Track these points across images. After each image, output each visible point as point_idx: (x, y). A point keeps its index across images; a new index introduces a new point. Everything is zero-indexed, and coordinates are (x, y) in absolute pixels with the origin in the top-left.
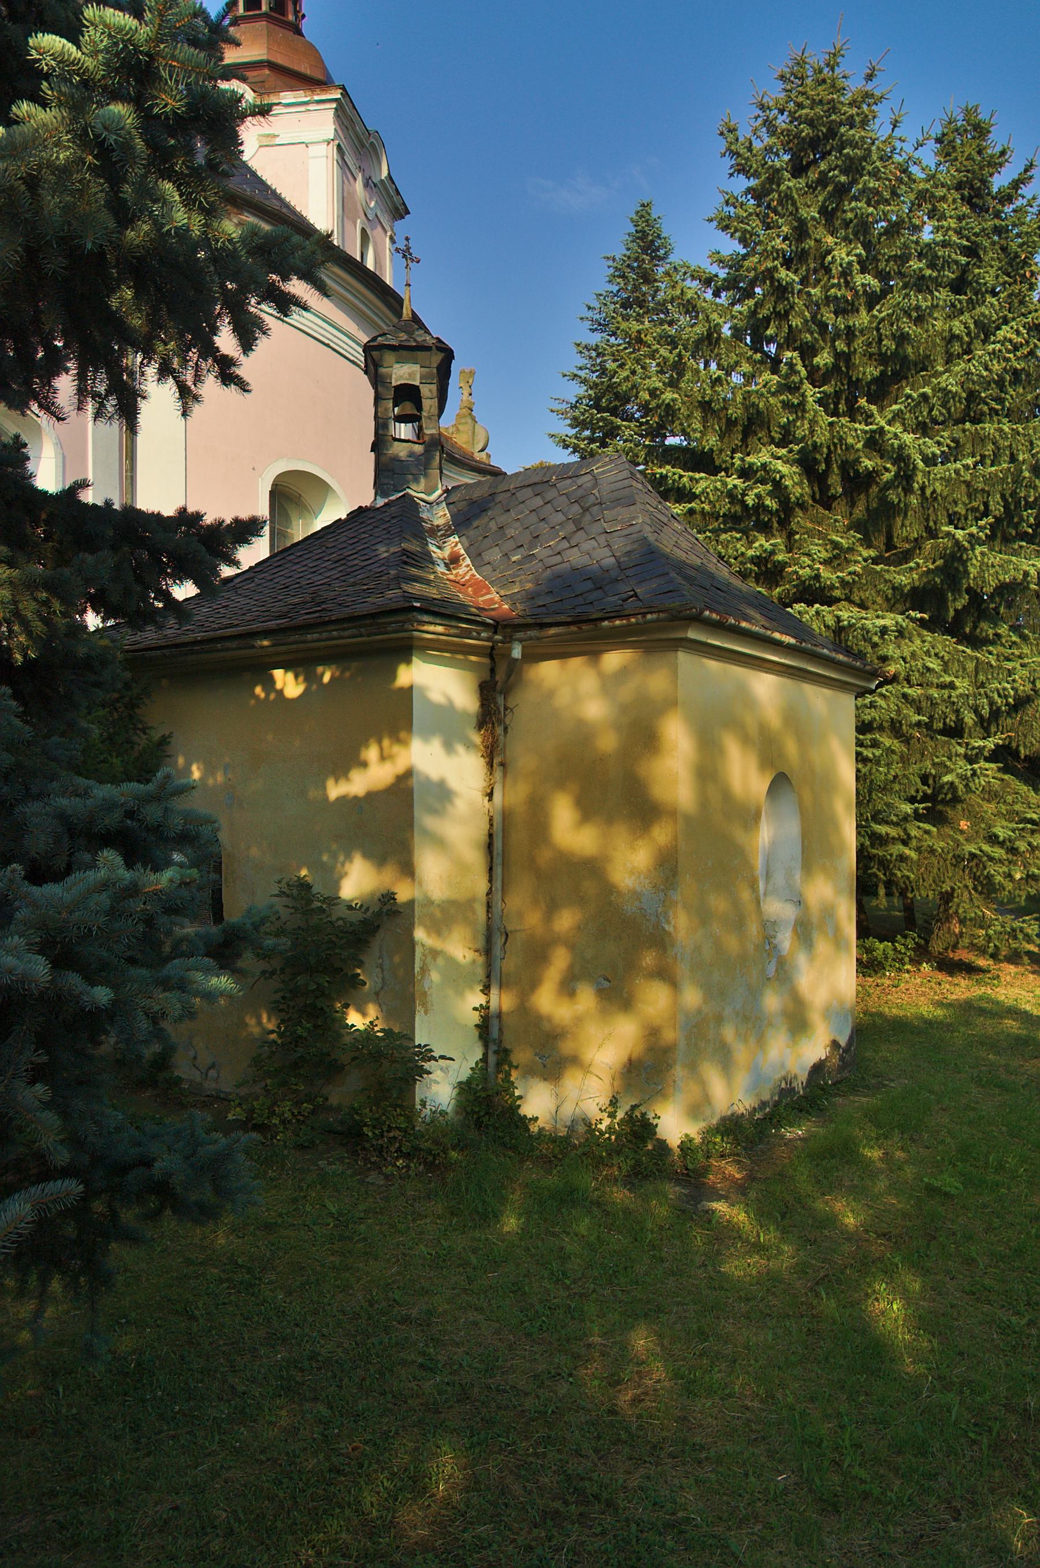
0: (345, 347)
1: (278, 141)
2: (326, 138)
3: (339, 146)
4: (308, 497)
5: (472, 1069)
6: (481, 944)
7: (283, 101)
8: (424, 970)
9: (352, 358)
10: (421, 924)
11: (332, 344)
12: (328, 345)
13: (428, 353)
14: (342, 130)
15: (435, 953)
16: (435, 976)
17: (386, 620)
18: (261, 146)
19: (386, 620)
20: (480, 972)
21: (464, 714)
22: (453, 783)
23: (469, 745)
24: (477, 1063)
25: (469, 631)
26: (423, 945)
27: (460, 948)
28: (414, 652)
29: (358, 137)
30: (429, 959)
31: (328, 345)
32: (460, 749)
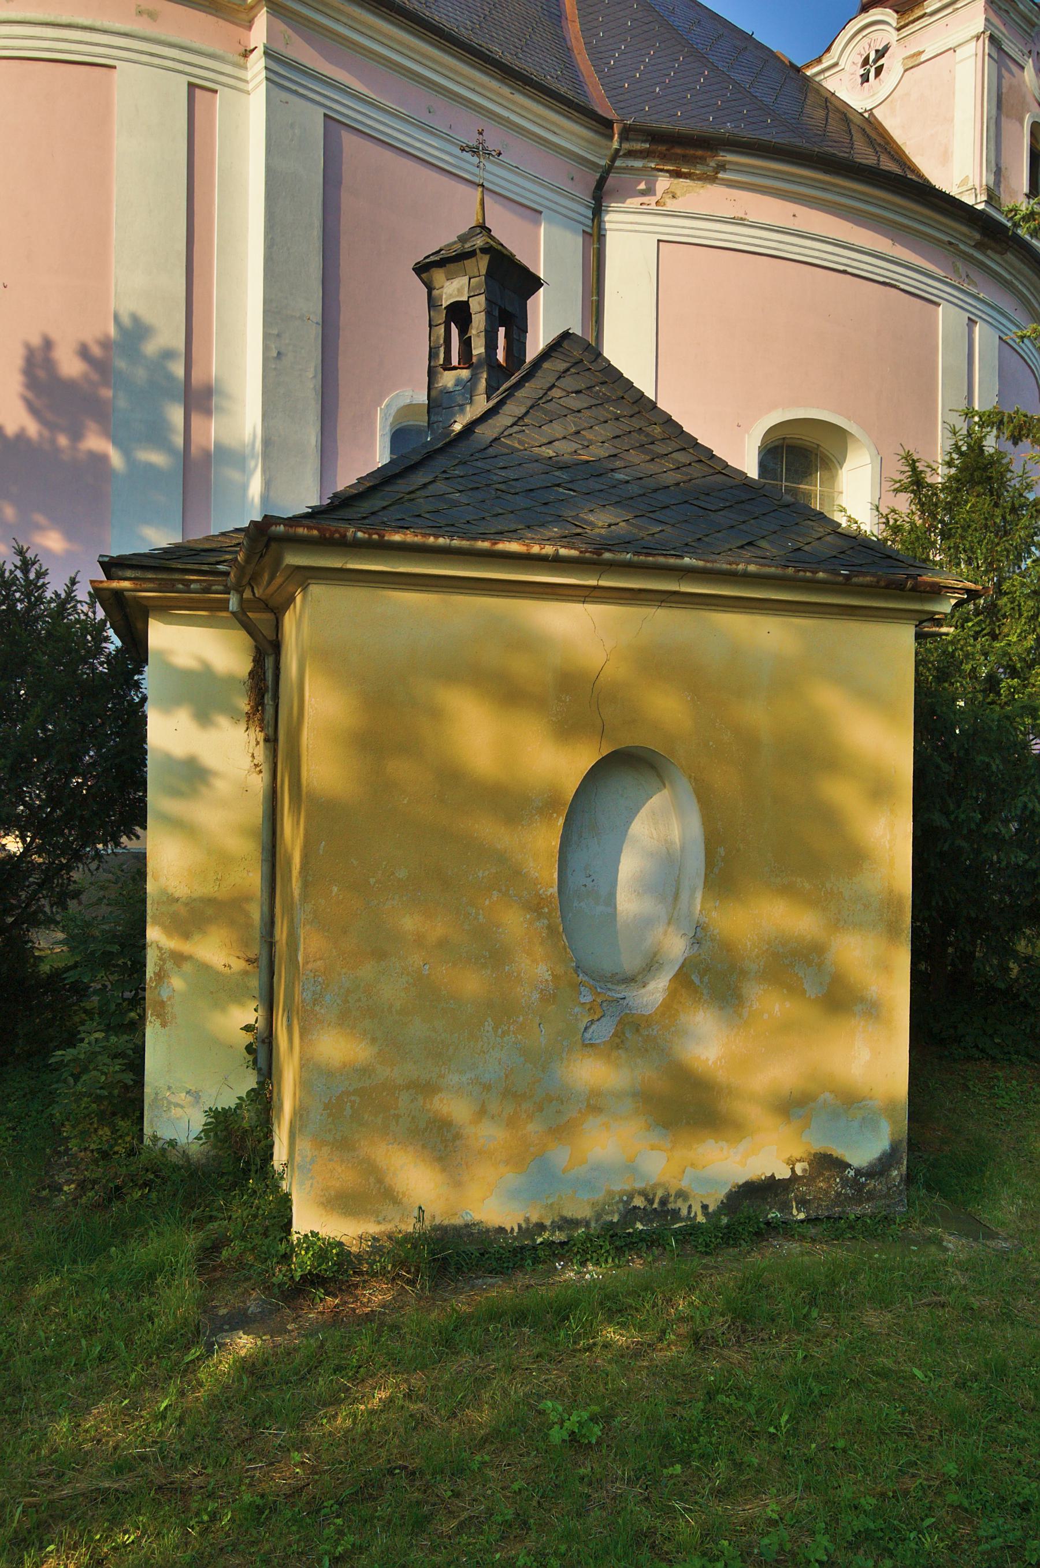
0: (870, 268)
1: (923, 58)
2: (974, 33)
3: (992, 38)
4: (827, 446)
5: (240, 1098)
6: (256, 949)
7: (928, 11)
8: (160, 976)
9: (882, 279)
10: (155, 923)
11: (849, 270)
12: (845, 272)
13: (473, 259)
14: (1000, 17)
15: (179, 958)
16: (177, 983)
17: (192, 577)
18: (906, 71)
19: (192, 577)
20: (254, 983)
21: (230, 680)
22: (210, 759)
23: (234, 716)
24: (248, 1093)
25: (211, 584)
26: (160, 948)
27: (217, 952)
28: (151, 614)
29: (1025, 18)
30: (169, 965)
31: (845, 272)
32: (223, 721)
